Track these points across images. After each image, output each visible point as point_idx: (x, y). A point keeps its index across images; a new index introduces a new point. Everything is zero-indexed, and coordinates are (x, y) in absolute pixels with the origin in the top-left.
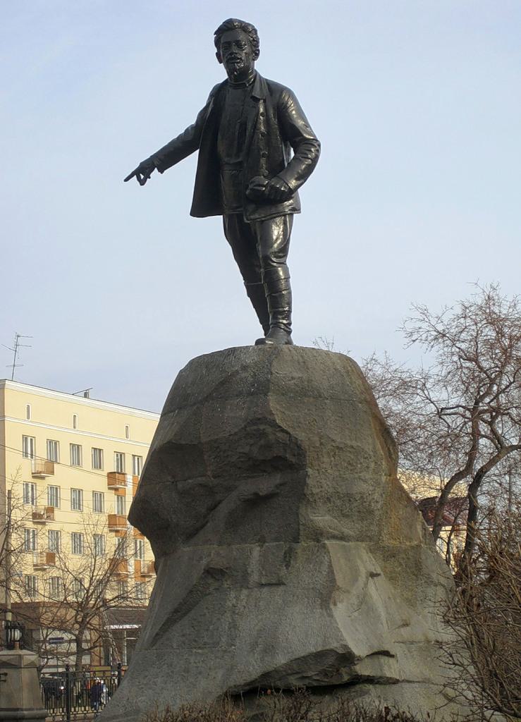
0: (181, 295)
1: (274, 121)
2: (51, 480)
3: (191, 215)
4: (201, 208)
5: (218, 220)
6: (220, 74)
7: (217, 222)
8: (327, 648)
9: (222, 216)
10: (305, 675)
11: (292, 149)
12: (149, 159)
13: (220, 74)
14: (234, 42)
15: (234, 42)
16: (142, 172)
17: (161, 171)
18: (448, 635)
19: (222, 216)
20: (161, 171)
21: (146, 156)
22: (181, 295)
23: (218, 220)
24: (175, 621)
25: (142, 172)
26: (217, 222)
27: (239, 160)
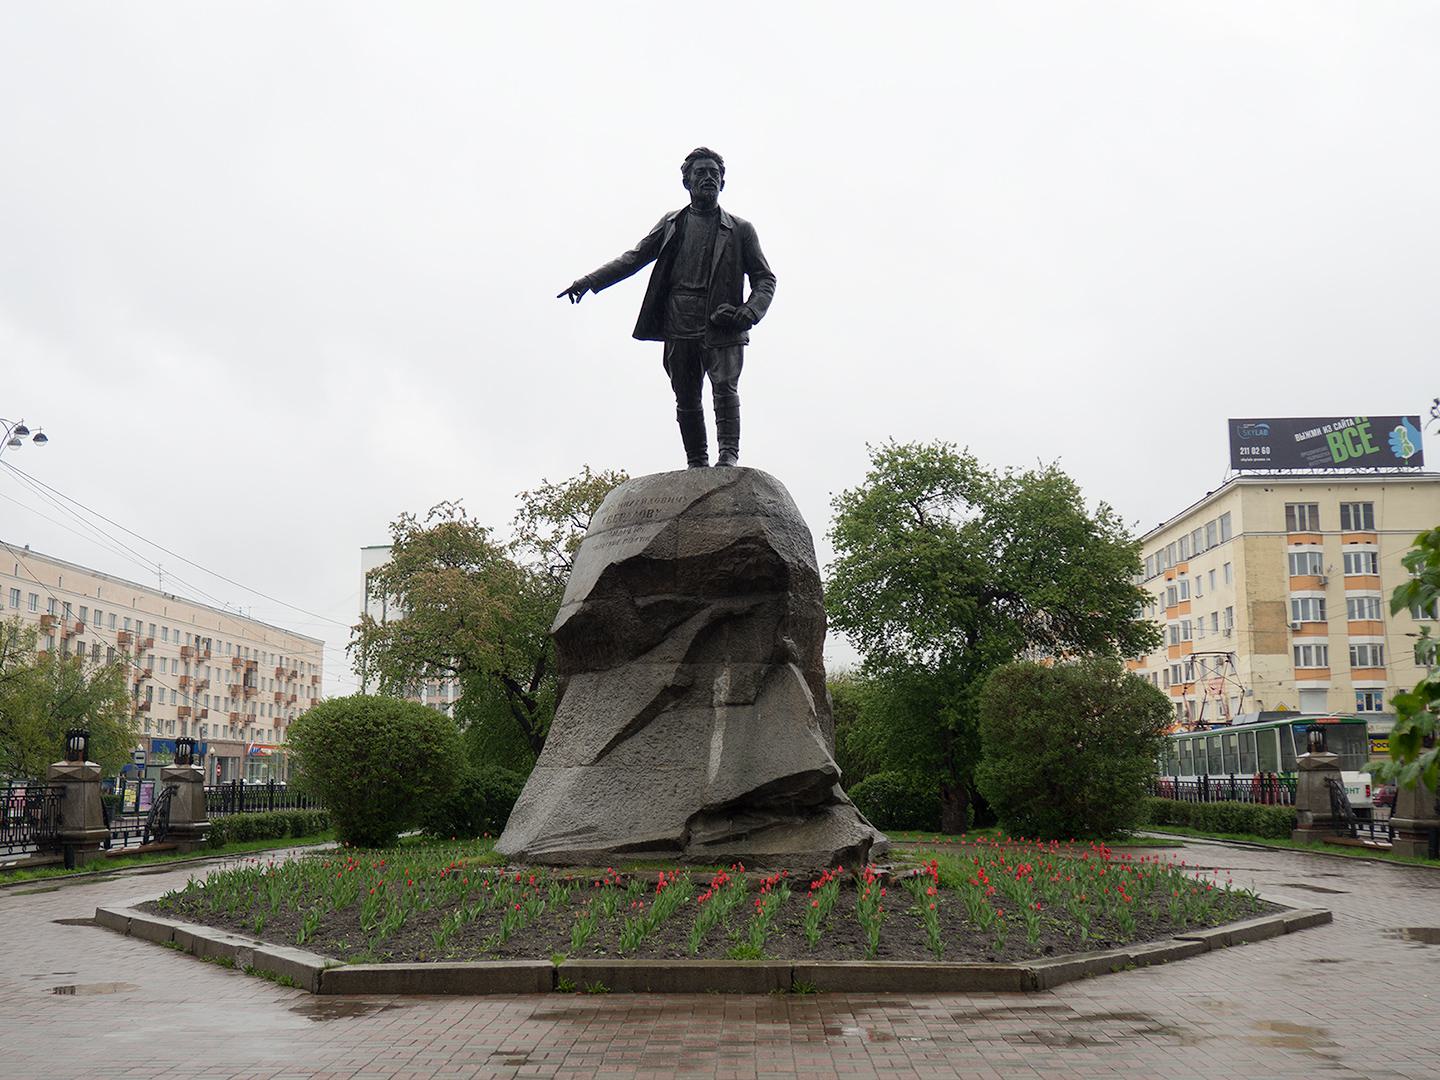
0: (622, 416)
1: (739, 254)
2: (79, 638)
3: (635, 336)
4: (645, 329)
5: (660, 346)
6: (682, 199)
7: (658, 347)
8: (763, 779)
9: (663, 343)
10: (784, 795)
11: (746, 277)
12: (583, 280)
13: (682, 199)
14: (703, 172)
15: (703, 172)
16: (577, 291)
17: (596, 292)
18: (731, 822)
19: (663, 343)
20: (596, 292)
21: (580, 276)
22: (622, 416)
23: (660, 346)
24: (626, 738)
25: (577, 291)
26: (658, 347)
27: (702, 286)
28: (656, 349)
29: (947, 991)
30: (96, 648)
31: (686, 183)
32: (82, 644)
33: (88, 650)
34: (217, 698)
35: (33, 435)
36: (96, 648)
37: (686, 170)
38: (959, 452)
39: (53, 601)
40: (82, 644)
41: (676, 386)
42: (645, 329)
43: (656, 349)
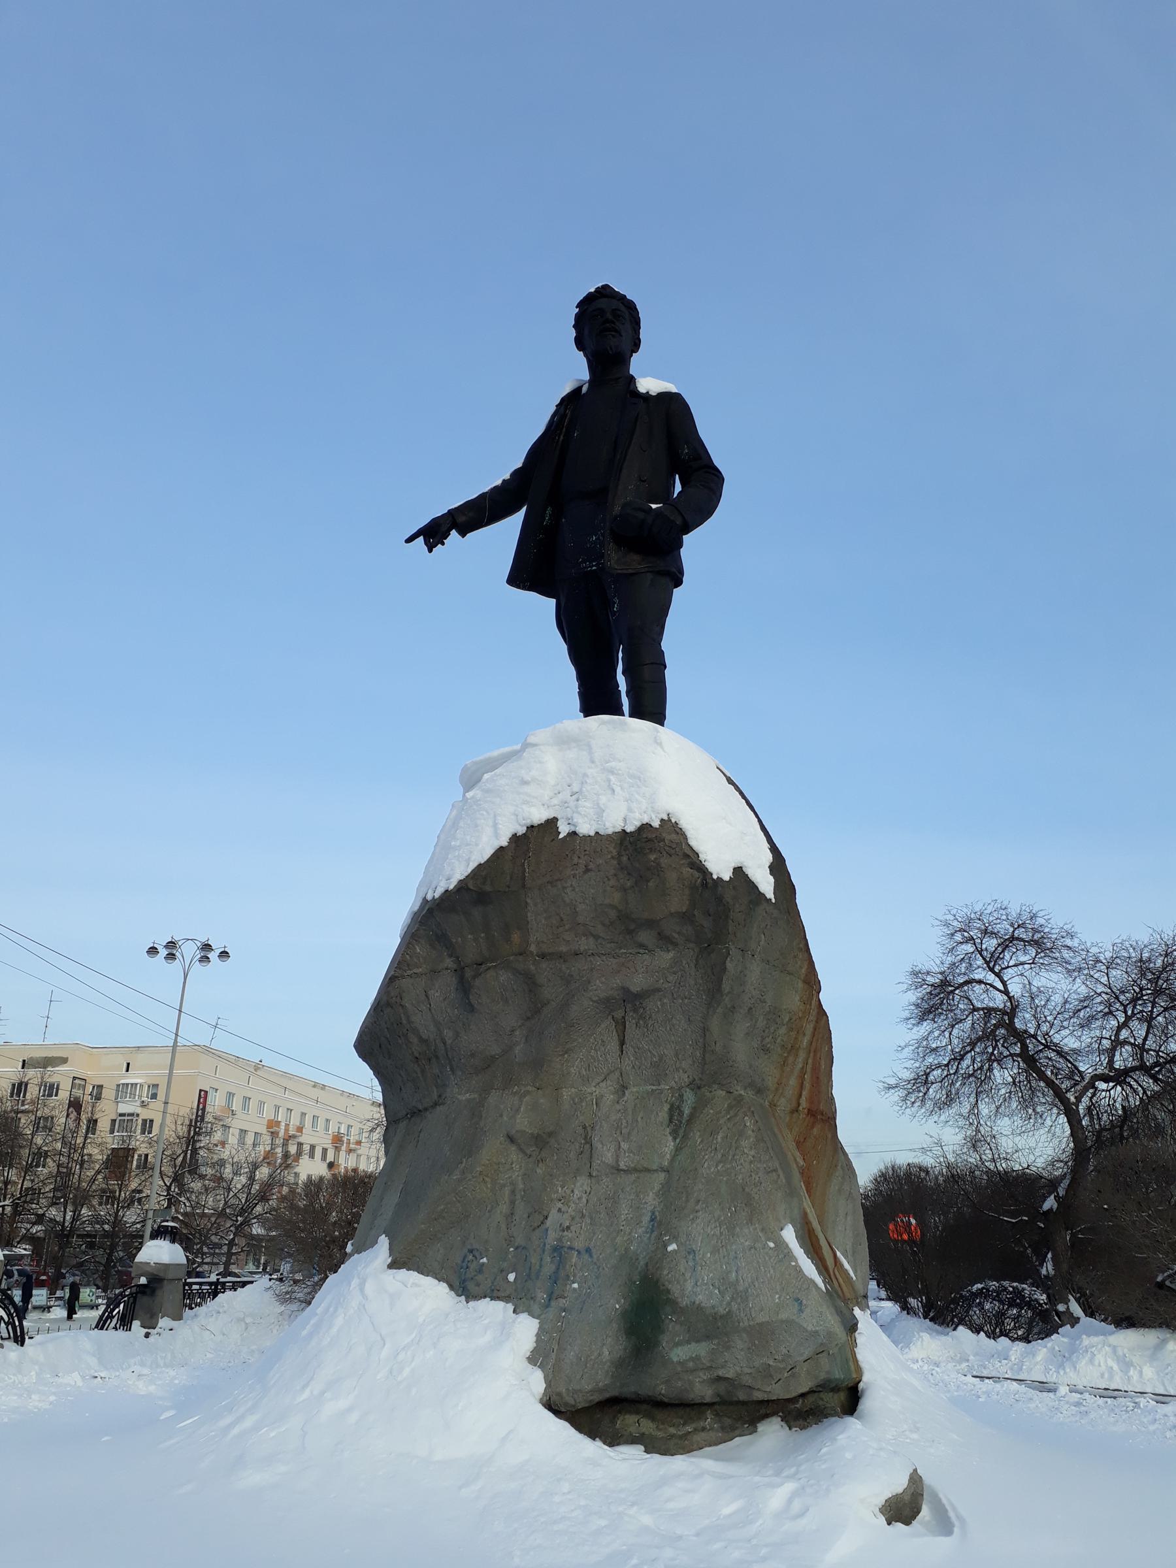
5: (554, 601)
13: (575, 370)
14: (606, 325)
15: (606, 325)
16: (433, 534)
17: (463, 533)
20: (463, 533)
25: (433, 534)
28: (592, 834)
29: (408, 947)
30: (313, 1147)
31: (580, 343)
32: (300, 1145)
33: (306, 1148)
34: (243, 1132)
35: (218, 952)
36: (313, 1147)
37: (580, 322)
38: (882, 1167)
39: (277, 1108)
40: (300, 1145)
41: (576, 656)
42: (525, 574)
43: (592, 834)
